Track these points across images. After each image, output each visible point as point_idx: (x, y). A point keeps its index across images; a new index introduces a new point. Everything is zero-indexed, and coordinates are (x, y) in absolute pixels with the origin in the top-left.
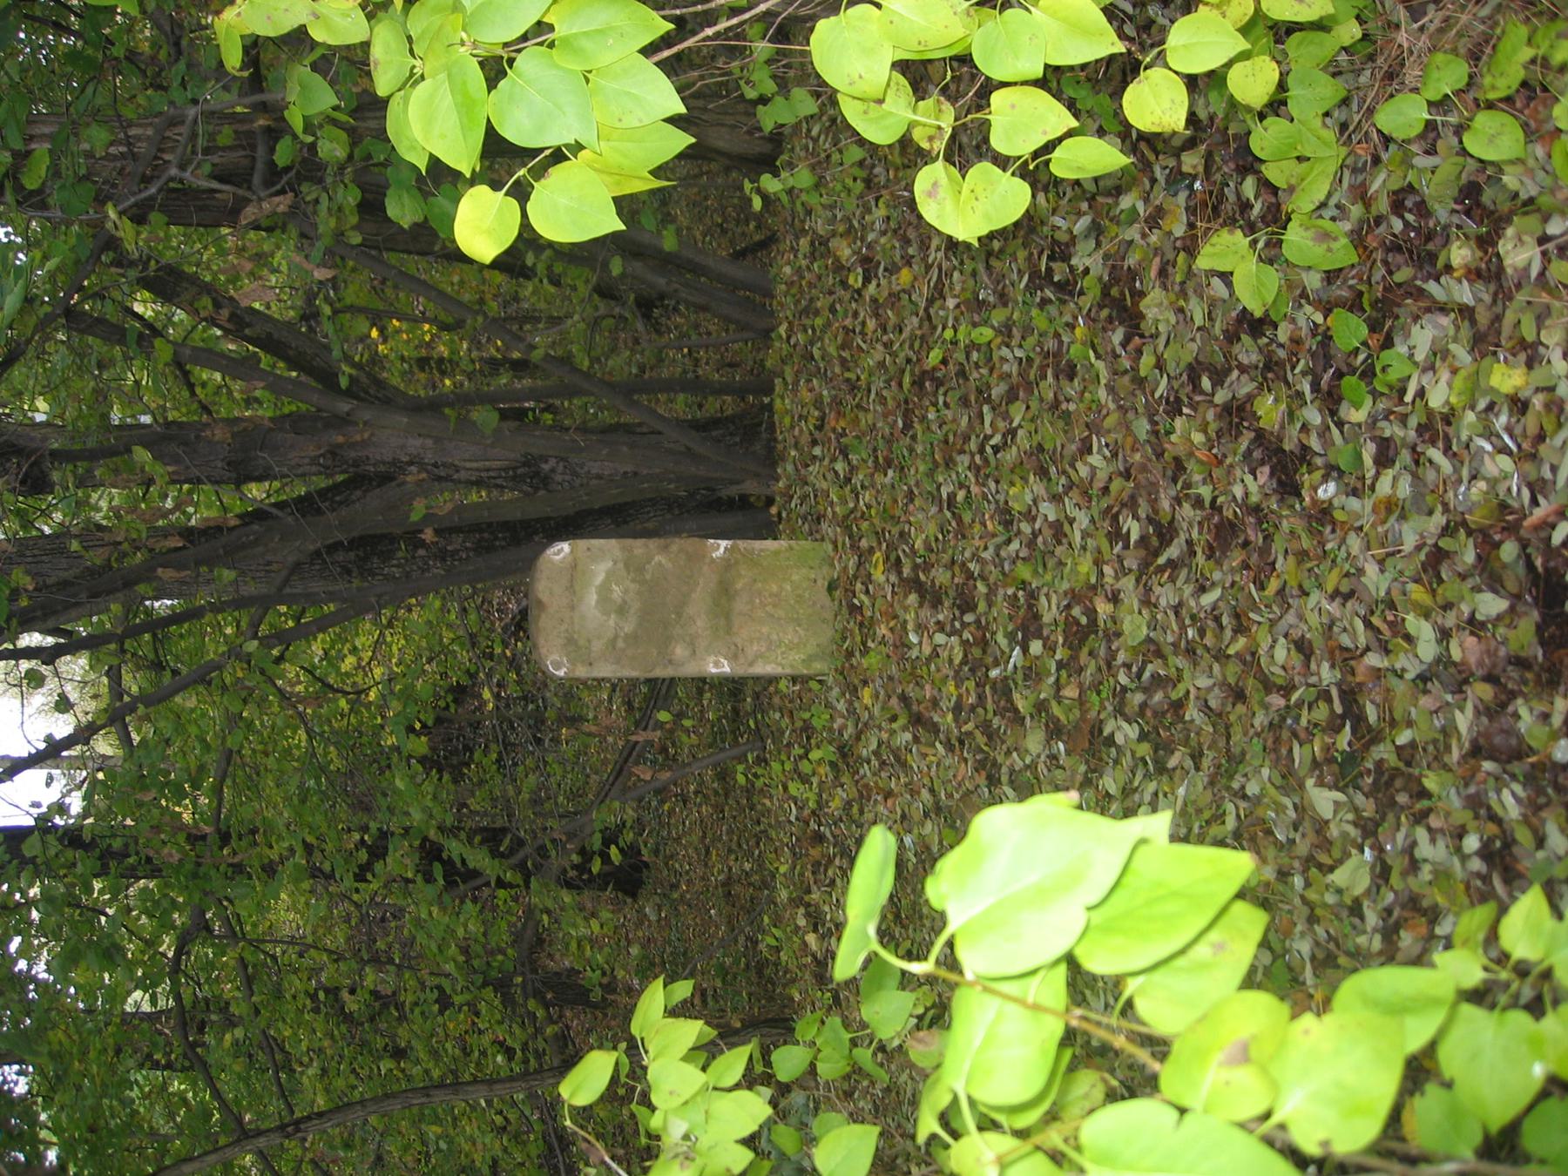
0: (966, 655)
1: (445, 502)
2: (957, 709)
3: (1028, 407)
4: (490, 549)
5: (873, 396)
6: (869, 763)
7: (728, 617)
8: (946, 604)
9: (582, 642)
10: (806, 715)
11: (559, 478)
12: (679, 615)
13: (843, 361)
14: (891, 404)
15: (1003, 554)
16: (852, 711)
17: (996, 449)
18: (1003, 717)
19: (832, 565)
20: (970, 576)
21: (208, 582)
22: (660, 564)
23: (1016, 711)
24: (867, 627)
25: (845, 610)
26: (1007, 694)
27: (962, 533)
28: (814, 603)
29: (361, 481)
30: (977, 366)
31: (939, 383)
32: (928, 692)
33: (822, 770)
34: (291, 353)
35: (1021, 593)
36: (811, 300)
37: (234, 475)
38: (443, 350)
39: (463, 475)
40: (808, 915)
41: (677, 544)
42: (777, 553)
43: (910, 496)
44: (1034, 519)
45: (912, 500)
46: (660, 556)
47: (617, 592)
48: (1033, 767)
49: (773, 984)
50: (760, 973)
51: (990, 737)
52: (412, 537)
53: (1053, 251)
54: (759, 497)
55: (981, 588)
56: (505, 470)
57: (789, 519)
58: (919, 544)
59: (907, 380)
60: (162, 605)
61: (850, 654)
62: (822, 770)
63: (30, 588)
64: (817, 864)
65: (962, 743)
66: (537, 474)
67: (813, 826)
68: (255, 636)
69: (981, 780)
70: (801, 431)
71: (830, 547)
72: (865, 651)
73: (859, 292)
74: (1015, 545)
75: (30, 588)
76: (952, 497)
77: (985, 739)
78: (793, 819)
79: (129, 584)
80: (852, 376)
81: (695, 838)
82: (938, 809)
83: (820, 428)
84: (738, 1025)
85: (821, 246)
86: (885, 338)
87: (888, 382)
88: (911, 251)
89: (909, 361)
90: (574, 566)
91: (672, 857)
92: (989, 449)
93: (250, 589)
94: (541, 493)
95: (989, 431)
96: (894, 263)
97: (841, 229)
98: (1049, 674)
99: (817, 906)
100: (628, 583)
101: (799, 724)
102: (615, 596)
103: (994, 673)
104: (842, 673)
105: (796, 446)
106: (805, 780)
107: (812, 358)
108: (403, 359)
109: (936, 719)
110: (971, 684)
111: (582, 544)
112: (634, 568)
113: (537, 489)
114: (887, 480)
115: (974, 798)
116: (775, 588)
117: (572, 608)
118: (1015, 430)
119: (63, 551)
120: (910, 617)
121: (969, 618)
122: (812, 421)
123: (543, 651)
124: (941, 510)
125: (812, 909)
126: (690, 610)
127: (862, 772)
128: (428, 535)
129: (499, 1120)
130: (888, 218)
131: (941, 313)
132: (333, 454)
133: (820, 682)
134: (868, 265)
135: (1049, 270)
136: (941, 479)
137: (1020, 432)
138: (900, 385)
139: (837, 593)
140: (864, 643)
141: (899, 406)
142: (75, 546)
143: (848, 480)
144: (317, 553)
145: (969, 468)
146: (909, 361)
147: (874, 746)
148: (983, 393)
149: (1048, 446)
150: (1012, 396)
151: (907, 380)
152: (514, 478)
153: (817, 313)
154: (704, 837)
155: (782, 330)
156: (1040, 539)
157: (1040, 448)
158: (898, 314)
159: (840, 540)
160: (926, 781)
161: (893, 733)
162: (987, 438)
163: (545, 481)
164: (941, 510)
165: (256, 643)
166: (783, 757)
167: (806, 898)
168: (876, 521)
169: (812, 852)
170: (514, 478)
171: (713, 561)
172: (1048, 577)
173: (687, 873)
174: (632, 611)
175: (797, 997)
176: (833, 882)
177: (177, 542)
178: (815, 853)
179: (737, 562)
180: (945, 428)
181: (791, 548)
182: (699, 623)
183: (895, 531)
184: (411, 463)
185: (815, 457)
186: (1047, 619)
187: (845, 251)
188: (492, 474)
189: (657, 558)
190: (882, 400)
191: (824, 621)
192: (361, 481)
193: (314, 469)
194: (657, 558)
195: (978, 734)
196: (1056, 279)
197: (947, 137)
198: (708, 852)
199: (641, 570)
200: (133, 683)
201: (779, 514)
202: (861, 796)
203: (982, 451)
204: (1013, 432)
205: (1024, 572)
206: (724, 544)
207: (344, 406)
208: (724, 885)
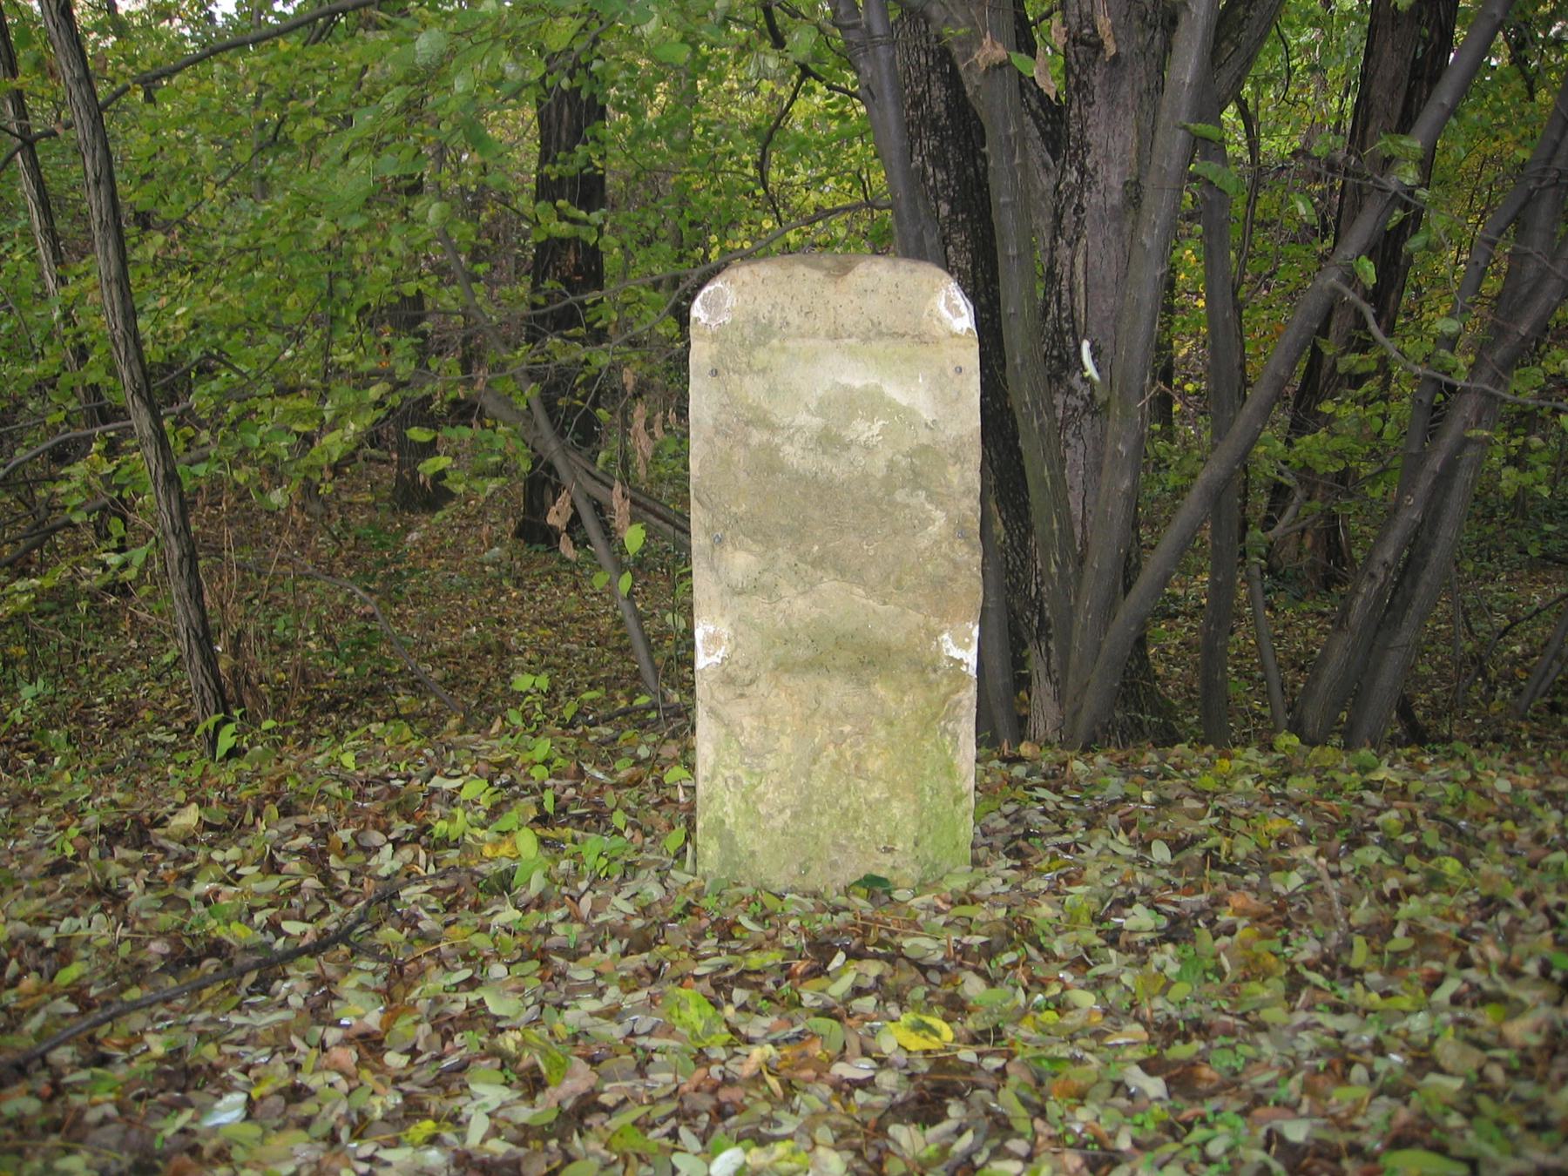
7: (810, 666)
9: (761, 356)
12: (818, 563)
14: (1341, 1097)
19: (922, 886)
22: (932, 521)
25: (825, 921)
28: (842, 849)
34: (1241, 10)
39: (1064, 252)
41: (970, 557)
42: (949, 770)
46: (946, 516)
47: (865, 430)
49: (347, 711)
50: (373, 692)
56: (1072, 318)
57: (1012, 782)
61: (726, 930)
71: (960, 883)
72: (720, 986)
78: (436, 781)
81: (572, 609)
90: (921, 339)
91: (556, 579)
101: (610, 799)
104: (689, 908)
105: (1162, 802)
107: (1355, 842)
112: (919, 470)
114: (1137, 1078)
116: (874, 765)
117: (835, 336)
126: (829, 585)
133: (680, 854)
139: (860, 902)
140: (741, 979)
141: (1340, 1124)
152: (1059, 331)
154: (572, 620)
159: (979, 913)
168: (1026, 1030)
170: (1059, 331)
171: (933, 635)
173: (532, 598)
174: (827, 462)
179: (929, 685)
181: (957, 800)
182: (800, 604)
183: (1008, 1102)
184: (1082, 171)
185: (1147, 846)
188: (1065, 297)
189: (940, 516)
190: (1340, 1061)
191: (805, 869)
193: (1074, 21)
194: (940, 516)
197: (972, 672)
198: (550, 624)
199: (916, 479)
201: (1019, 760)
206: (970, 657)
208: (501, 645)
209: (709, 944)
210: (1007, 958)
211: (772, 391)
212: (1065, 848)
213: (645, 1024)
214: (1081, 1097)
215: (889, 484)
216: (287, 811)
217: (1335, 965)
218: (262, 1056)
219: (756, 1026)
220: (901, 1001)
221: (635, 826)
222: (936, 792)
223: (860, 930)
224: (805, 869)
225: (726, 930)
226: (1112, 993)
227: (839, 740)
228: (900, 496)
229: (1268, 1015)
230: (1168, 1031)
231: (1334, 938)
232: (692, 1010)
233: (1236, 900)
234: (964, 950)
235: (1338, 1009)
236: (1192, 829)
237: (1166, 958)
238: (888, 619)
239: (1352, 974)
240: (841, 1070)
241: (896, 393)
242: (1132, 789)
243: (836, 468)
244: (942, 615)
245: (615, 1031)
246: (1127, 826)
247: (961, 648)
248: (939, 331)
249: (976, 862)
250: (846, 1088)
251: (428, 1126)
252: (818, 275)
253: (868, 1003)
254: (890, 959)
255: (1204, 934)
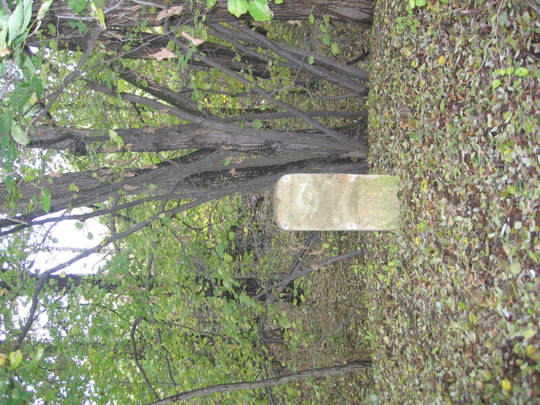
0: (474, 227)
1: (241, 159)
2: (469, 250)
3: (514, 114)
4: (251, 177)
5: (422, 113)
6: (417, 269)
7: (356, 206)
8: (463, 203)
9: (296, 216)
10: (386, 247)
11: (278, 150)
12: (336, 205)
13: (407, 100)
14: (433, 116)
15: (497, 181)
16: (409, 247)
17: (494, 134)
18: (497, 256)
19: (399, 185)
20: (478, 191)
21: (146, 189)
22: (328, 184)
23: (504, 253)
24: (418, 212)
26: (500, 245)
27: (472, 172)
29: (204, 150)
30: (482, 97)
31: (461, 106)
32: (452, 241)
33: (392, 270)
35: (508, 200)
36: (391, 75)
37: (156, 148)
38: (230, 106)
39: (242, 149)
40: (385, 329)
41: (335, 176)
42: (376, 180)
43: (442, 156)
44: (517, 166)
45: (443, 158)
46: (328, 180)
47: (310, 196)
48: (514, 280)
50: (349, 338)
51: (487, 264)
52: (225, 172)
53: (535, 38)
54: (355, 159)
55: (483, 197)
57: (378, 167)
58: (447, 177)
59: (442, 105)
60: (130, 198)
61: (408, 223)
62: (392, 270)
63: (78, 191)
64: (389, 308)
65: (470, 265)
66: (270, 148)
67: (388, 292)
68: (163, 211)
69: (482, 283)
70: (385, 130)
72: (417, 222)
73: (416, 69)
74: (505, 177)
75: (78, 191)
76: (467, 157)
77: (484, 265)
78: (378, 288)
79: (115, 190)
80: (411, 105)
81: (323, 286)
82: (455, 293)
83: (394, 128)
84: (346, 363)
85: (395, 51)
86: (430, 88)
87: (432, 107)
88: (444, 49)
89: (443, 97)
90: (292, 185)
92: (490, 134)
93: (161, 192)
94: (272, 156)
95: (490, 125)
96: (435, 55)
97: (406, 43)
98: (526, 238)
99: (389, 326)
100: (315, 192)
101: (382, 250)
102: (309, 197)
103: (491, 236)
106: (385, 273)
107: (391, 99)
108: (216, 109)
109: (455, 253)
110: (477, 240)
111: (296, 175)
112: (318, 185)
113: (270, 154)
114: (431, 149)
115: (478, 290)
116: (375, 194)
117: (292, 202)
118: (506, 125)
119: (90, 177)
120: (442, 209)
121: (476, 210)
122: (390, 126)
123: (280, 219)
124: (461, 161)
125: (386, 326)
126: (340, 203)
127: (414, 272)
128: (233, 172)
129: (251, 392)
130: (432, 36)
131: (462, 74)
132: (193, 140)
134: (421, 57)
135: (532, 48)
136: (461, 148)
137: (508, 126)
138: (439, 108)
139: (402, 197)
140: (416, 219)
141: (437, 117)
142: (94, 175)
143: (409, 150)
144: (187, 179)
145: (478, 143)
146: (443, 97)
147: (421, 262)
148: (486, 110)
149: (528, 132)
150: (504, 109)
151: (442, 105)
152: (261, 150)
153: (394, 80)
154: (326, 285)
155: (376, 88)
156: (520, 176)
157: (523, 131)
158: (437, 78)
159: (404, 175)
160: (449, 280)
161: (431, 258)
162: (489, 129)
163: (272, 151)
164: (461, 161)
165: (164, 214)
166: (374, 263)
167: (384, 322)
168: (424, 167)
169: (387, 303)
170: (261, 150)
171: (350, 183)
172: (525, 193)
175: (375, 358)
176: (397, 317)
177: (131, 175)
178: (389, 304)
179: (360, 184)
180: (464, 126)
183: (434, 171)
184: (222, 144)
185: (391, 140)
186: (525, 212)
187: (408, 53)
190: (428, 115)
191: (396, 208)
192: (204, 150)
193: (186, 146)
195: (481, 263)
196: (536, 51)
198: (328, 291)
199: (320, 186)
200: (119, 227)
201: (372, 164)
202: (413, 283)
203: (485, 135)
204: (504, 126)
205: (512, 190)
206: (355, 176)
207: (198, 120)
208: (334, 304)
209: (410, 226)
210: (412, 170)
211: (302, 214)
212: (392, 157)
213: (423, 235)
214: (434, 158)
215: (321, 191)
216: (385, 319)
217: (413, 110)
218: (430, 303)
219: (424, 215)
220: (420, 189)
221: (388, 244)
222: (381, 182)
223: (407, 198)
224: (396, 208)
225: (408, 223)
226: (418, 151)
227: (371, 202)
228: (323, 189)
229: (421, 125)
230: (424, 142)
231: (408, 110)
232: (421, 226)
233: (401, 126)
234: (411, 178)
235: (420, 111)
236: (388, 131)
237: (412, 140)
238: (347, 192)
239: (415, 107)
240: (430, 199)
241: (303, 190)
242: (379, 141)
243: (318, 201)
244: (346, 181)
245: (425, 240)
246: (388, 144)
247: (352, 177)
248: (291, 182)
249: (395, 174)
250: (433, 198)
251: (440, 269)
252: (280, 205)
253: (420, 195)
254: (412, 191)
255: (408, 133)
